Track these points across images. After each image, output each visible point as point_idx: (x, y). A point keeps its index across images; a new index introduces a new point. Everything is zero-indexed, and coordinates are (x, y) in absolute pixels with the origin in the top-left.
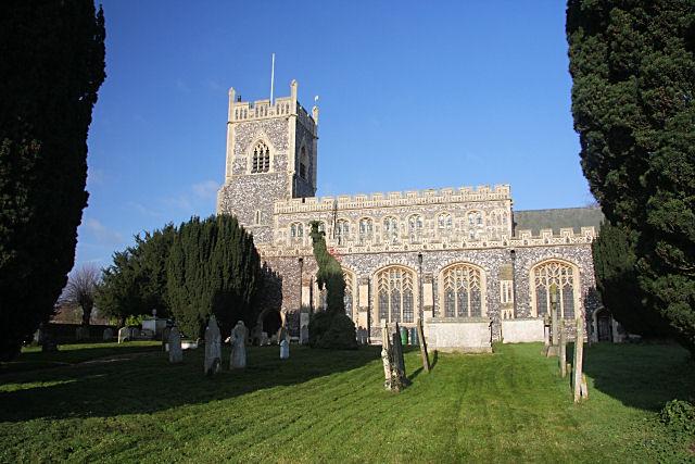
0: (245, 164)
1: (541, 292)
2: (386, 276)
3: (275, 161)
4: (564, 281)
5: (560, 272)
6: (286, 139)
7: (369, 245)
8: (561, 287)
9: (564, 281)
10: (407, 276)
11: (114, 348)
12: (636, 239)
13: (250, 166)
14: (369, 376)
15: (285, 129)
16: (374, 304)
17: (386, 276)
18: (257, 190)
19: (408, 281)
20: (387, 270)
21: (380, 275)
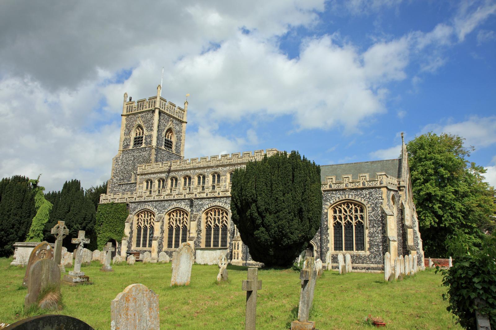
0: (130, 142)
1: (337, 226)
2: (211, 214)
3: (146, 139)
4: (356, 218)
5: (353, 211)
6: (152, 124)
7: (164, 195)
8: (354, 222)
9: (356, 218)
10: (225, 214)
11: (179, 241)
12: (30, 232)
13: (132, 143)
14: (365, 268)
15: (152, 118)
16: (166, 235)
17: (211, 214)
18: (134, 159)
19: (224, 218)
20: (173, 212)
21: (207, 214)
